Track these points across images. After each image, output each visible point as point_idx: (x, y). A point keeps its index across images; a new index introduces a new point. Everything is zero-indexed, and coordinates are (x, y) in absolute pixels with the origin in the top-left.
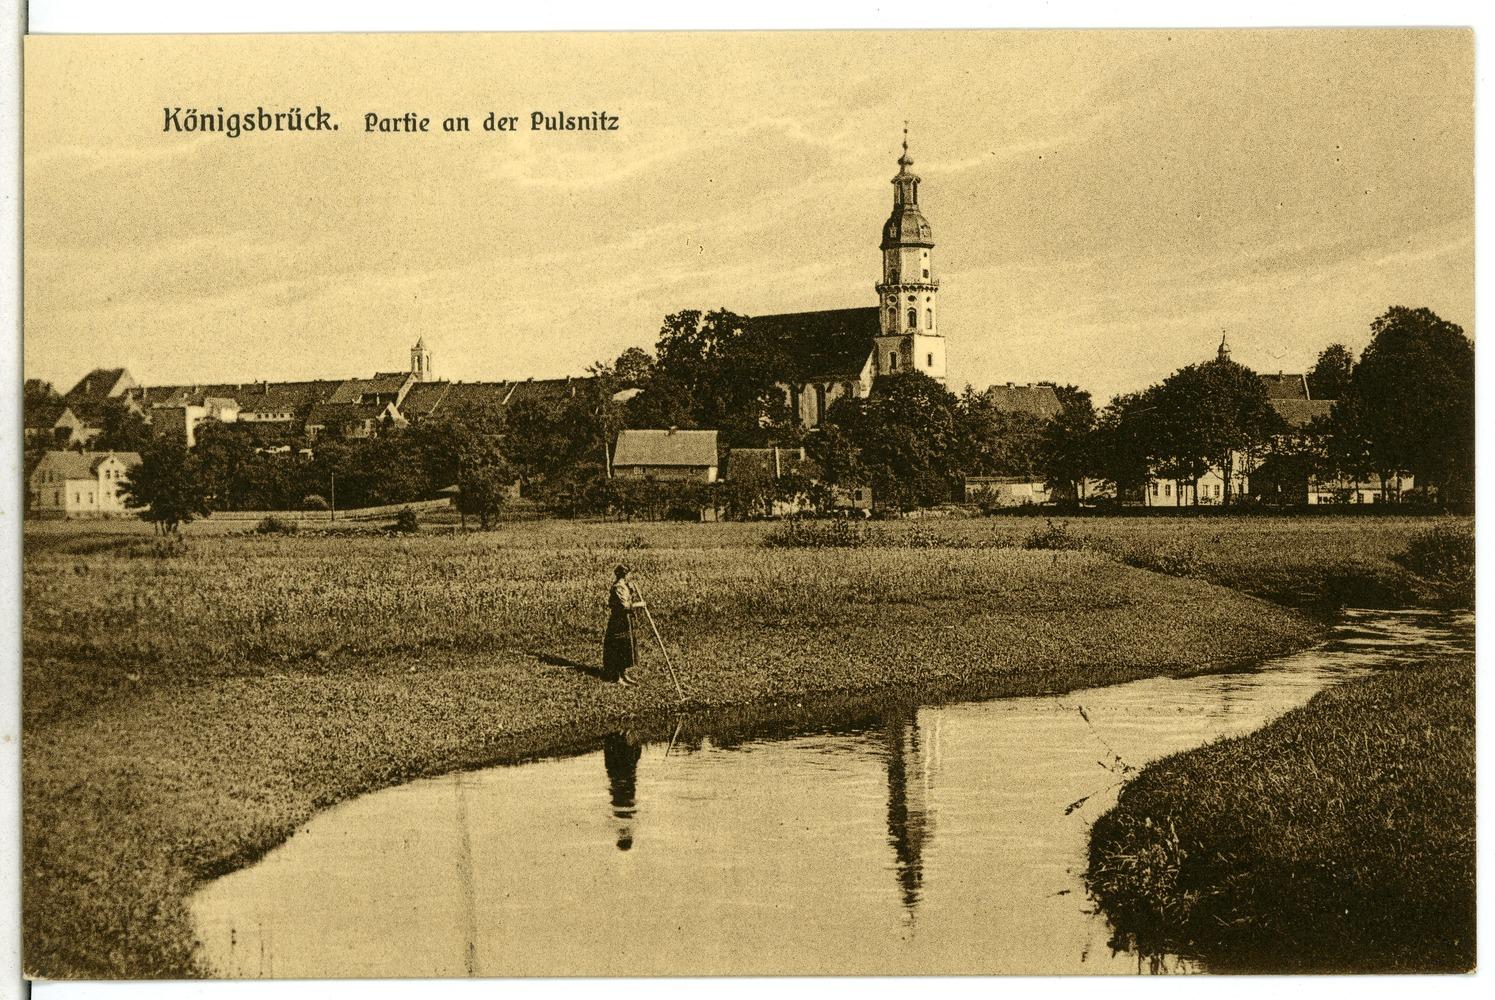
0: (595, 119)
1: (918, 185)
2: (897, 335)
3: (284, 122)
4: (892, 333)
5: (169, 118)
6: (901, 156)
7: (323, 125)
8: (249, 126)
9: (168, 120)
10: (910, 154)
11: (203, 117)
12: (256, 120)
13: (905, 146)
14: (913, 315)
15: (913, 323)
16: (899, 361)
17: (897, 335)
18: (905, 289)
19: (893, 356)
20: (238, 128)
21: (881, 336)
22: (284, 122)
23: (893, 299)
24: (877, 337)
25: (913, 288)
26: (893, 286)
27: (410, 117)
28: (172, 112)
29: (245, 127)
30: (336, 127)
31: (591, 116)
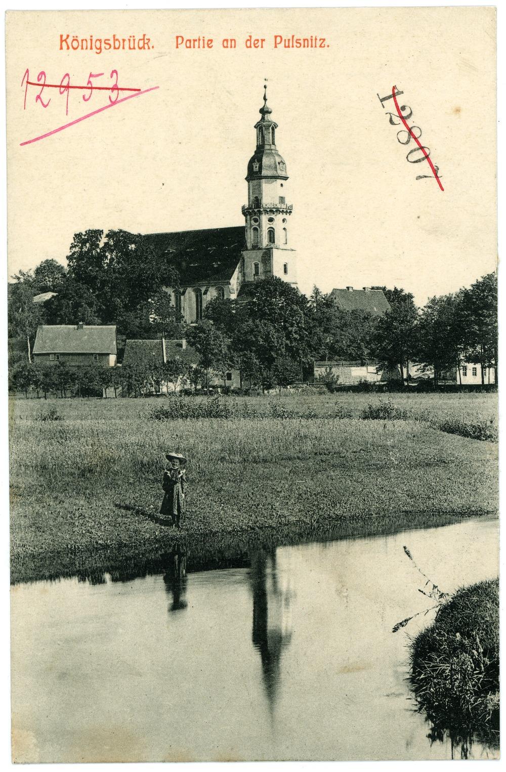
0: (91, 40)
1: (276, 130)
2: (260, 249)
6: (262, 107)
7: (64, 43)
8: (108, 47)
9: (62, 41)
10: (270, 105)
11: (82, 40)
12: (111, 42)
13: (265, 99)
14: (271, 232)
15: (272, 239)
16: (261, 270)
18: (266, 212)
19: (256, 266)
20: (100, 48)
21: (247, 250)
23: (256, 221)
24: (243, 251)
25: (271, 211)
26: (256, 210)
27: (201, 38)
28: (64, 38)
30: (153, 47)
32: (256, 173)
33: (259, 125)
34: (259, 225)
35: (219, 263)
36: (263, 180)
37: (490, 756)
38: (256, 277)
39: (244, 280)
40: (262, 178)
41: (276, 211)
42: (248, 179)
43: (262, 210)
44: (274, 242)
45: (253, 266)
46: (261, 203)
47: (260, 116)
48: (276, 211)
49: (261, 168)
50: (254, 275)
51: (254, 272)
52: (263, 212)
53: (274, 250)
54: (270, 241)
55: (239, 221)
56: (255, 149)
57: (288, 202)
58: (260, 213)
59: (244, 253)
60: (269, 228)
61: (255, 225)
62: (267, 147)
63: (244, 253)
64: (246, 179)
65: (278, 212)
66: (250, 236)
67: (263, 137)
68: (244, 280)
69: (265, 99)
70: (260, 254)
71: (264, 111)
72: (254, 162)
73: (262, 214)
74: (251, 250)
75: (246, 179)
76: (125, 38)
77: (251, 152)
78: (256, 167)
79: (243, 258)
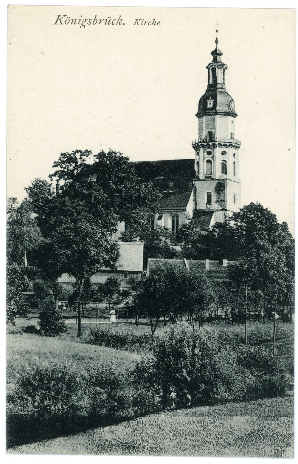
1: (226, 71)
2: (213, 179)
4: (208, 178)
6: (214, 49)
10: (221, 48)
13: (217, 42)
15: (224, 170)
17: (213, 179)
18: (220, 145)
19: (209, 196)
23: (209, 153)
25: (226, 146)
26: (210, 143)
32: (211, 109)
33: (212, 65)
34: (213, 158)
35: (145, 184)
36: (217, 116)
37: (107, 274)
38: (208, 206)
39: (196, 207)
40: (216, 114)
41: (230, 145)
42: (199, 115)
43: (217, 143)
44: (226, 173)
45: (206, 196)
46: (214, 137)
47: (212, 58)
48: (230, 145)
49: (215, 104)
50: (207, 204)
51: (206, 201)
52: (217, 146)
53: (228, 181)
54: (222, 172)
55: (189, 154)
56: (206, 88)
57: (236, 137)
58: (214, 146)
59: (196, 183)
60: (222, 161)
61: (209, 157)
62: (219, 86)
63: (196, 183)
64: (196, 115)
65: (231, 146)
66: (202, 170)
67: (215, 77)
68: (196, 207)
69: (217, 42)
70: (214, 184)
71: (215, 54)
72: (209, 99)
73: (216, 147)
74: (204, 180)
75: (196, 115)
76: (26, 197)
77: (203, 89)
78: (210, 104)
79: (195, 187)
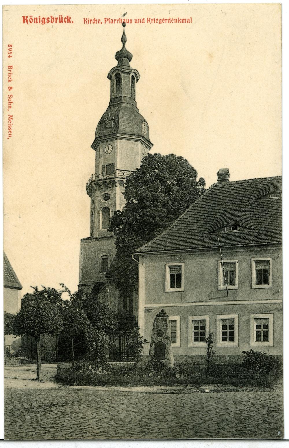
0: (40, 19)
3: (58, 21)
5: (25, 19)
7: (85, 22)
10: (129, 47)
13: (124, 40)
22: (58, 21)
29: (11, 133)
30: (73, 22)
31: (38, 18)
69: (124, 40)
